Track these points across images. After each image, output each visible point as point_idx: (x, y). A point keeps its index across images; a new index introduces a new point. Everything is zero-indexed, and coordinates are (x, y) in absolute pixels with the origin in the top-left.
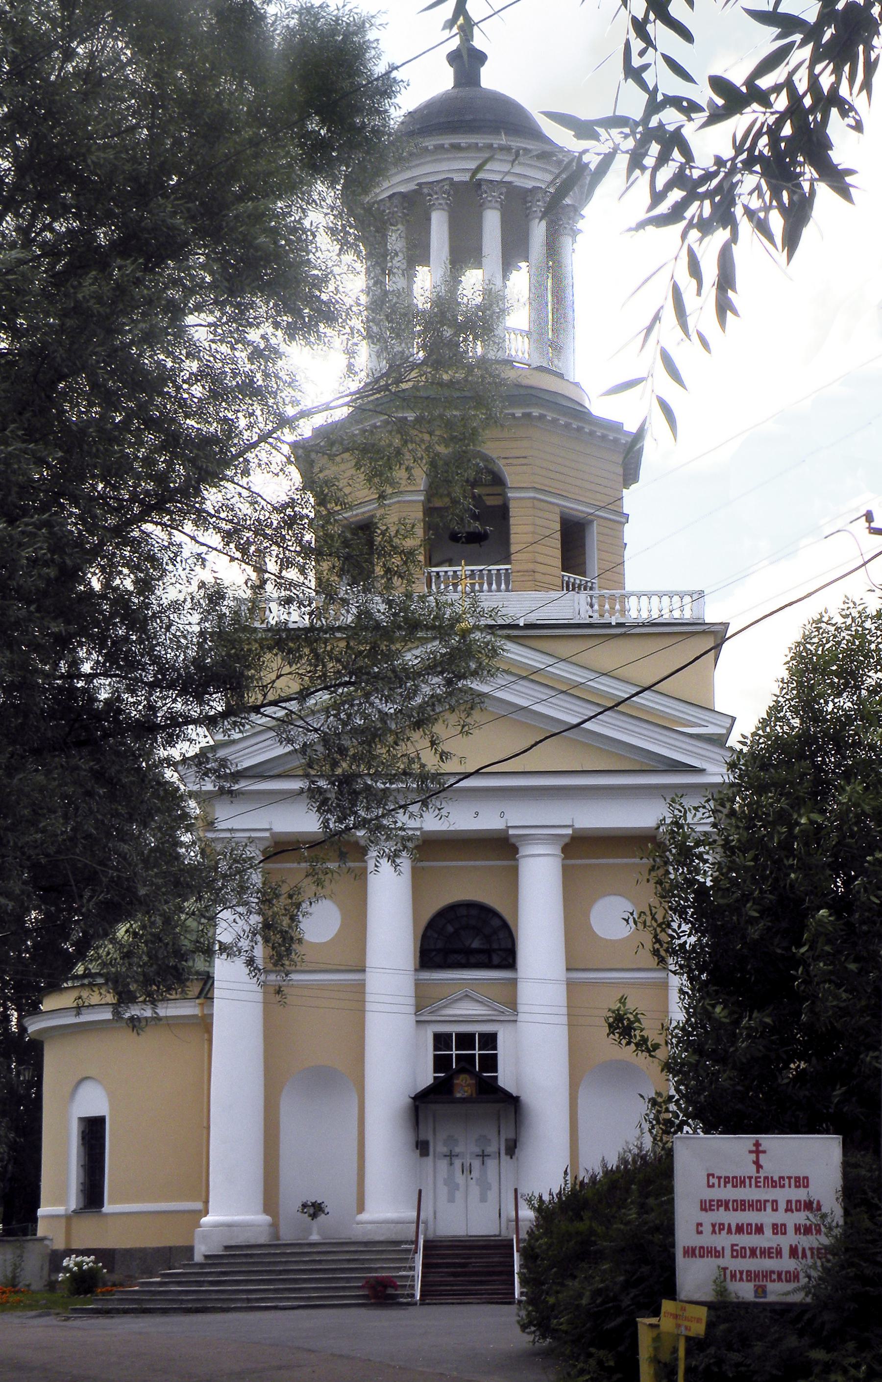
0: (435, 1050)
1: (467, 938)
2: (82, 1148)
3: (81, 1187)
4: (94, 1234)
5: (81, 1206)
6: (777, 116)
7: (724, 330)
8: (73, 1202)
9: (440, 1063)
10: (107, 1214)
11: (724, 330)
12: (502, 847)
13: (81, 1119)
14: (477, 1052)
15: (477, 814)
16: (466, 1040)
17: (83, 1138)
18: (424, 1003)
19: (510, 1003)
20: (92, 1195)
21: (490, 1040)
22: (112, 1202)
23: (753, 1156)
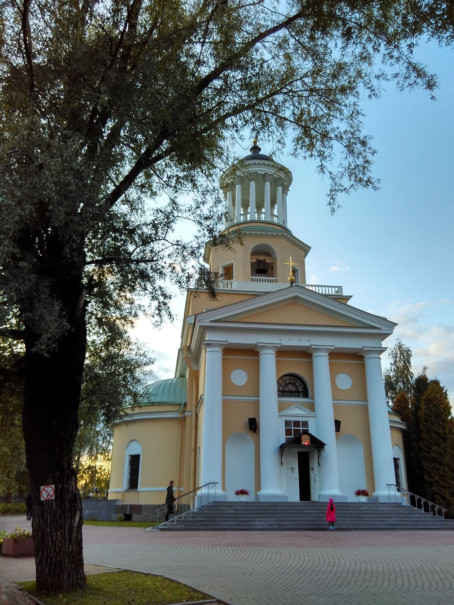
0: (286, 426)
1: (295, 386)
2: (129, 467)
3: (128, 481)
4: (131, 500)
5: (128, 488)
6: (80, 399)
7: (352, 296)
8: (125, 485)
9: (288, 432)
10: (139, 492)
11: (352, 296)
12: (306, 354)
13: (130, 455)
14: (301, 428)
15: (300, 340)
16: (297, 424)
17: (130, 463)
18: (281, 407)
19: (312, 407)
20: (133, 483)
21: (306, 424)
22: (141, 487)
23: (252, 3)
